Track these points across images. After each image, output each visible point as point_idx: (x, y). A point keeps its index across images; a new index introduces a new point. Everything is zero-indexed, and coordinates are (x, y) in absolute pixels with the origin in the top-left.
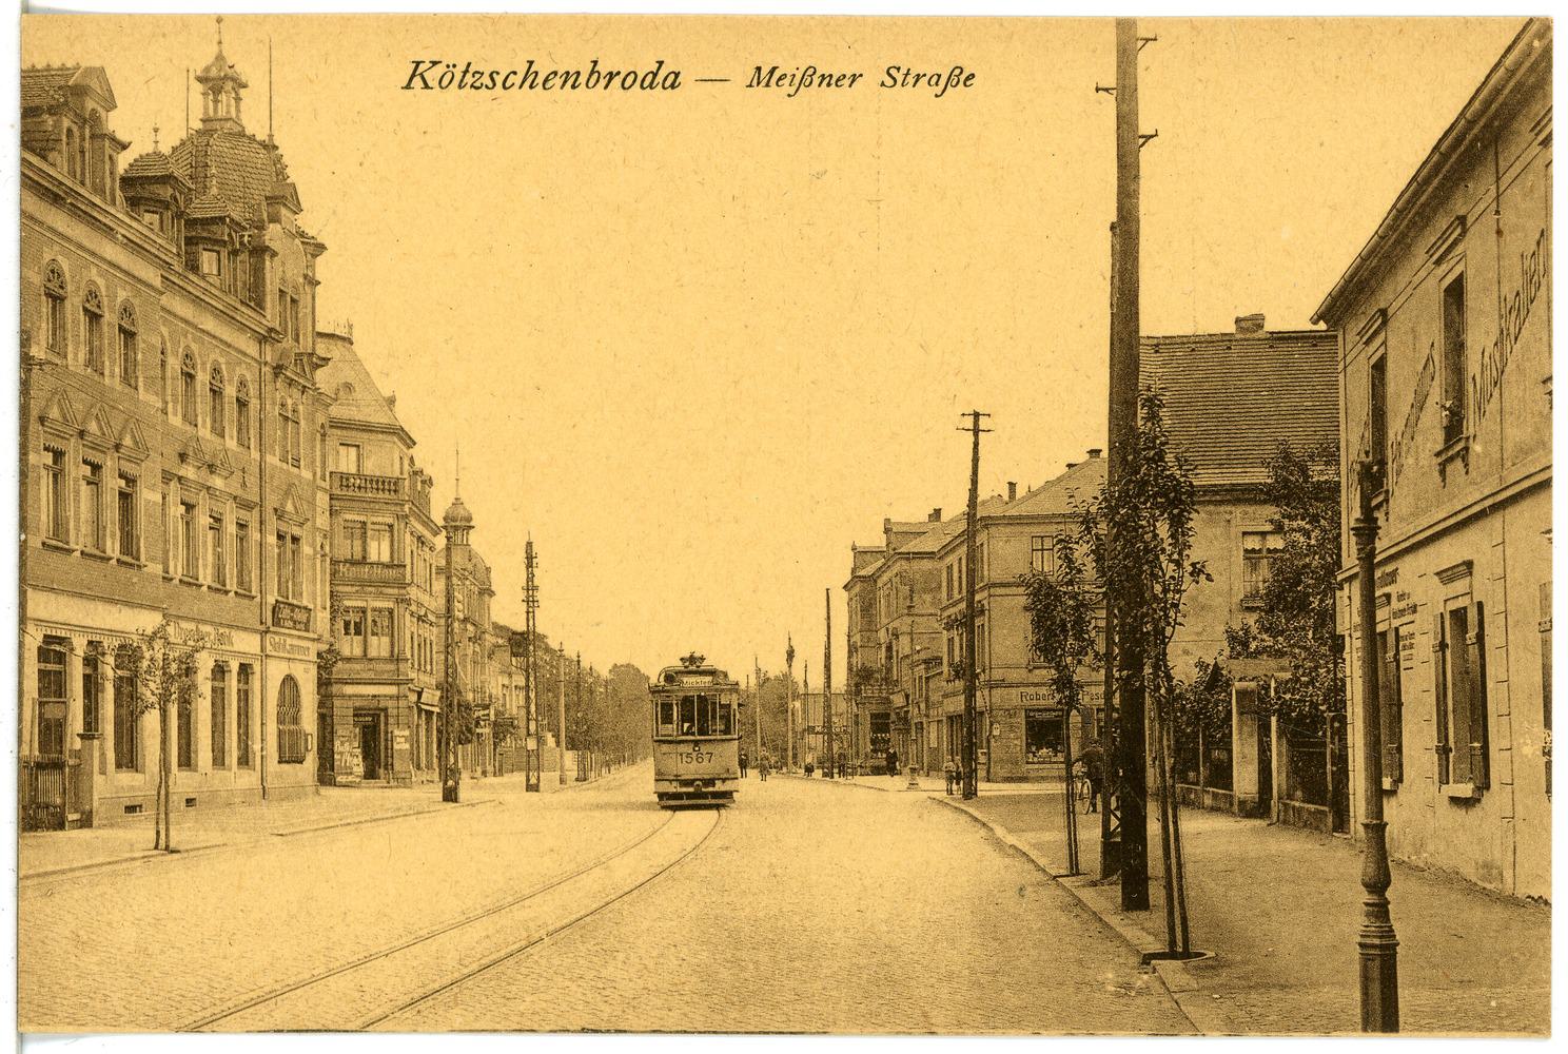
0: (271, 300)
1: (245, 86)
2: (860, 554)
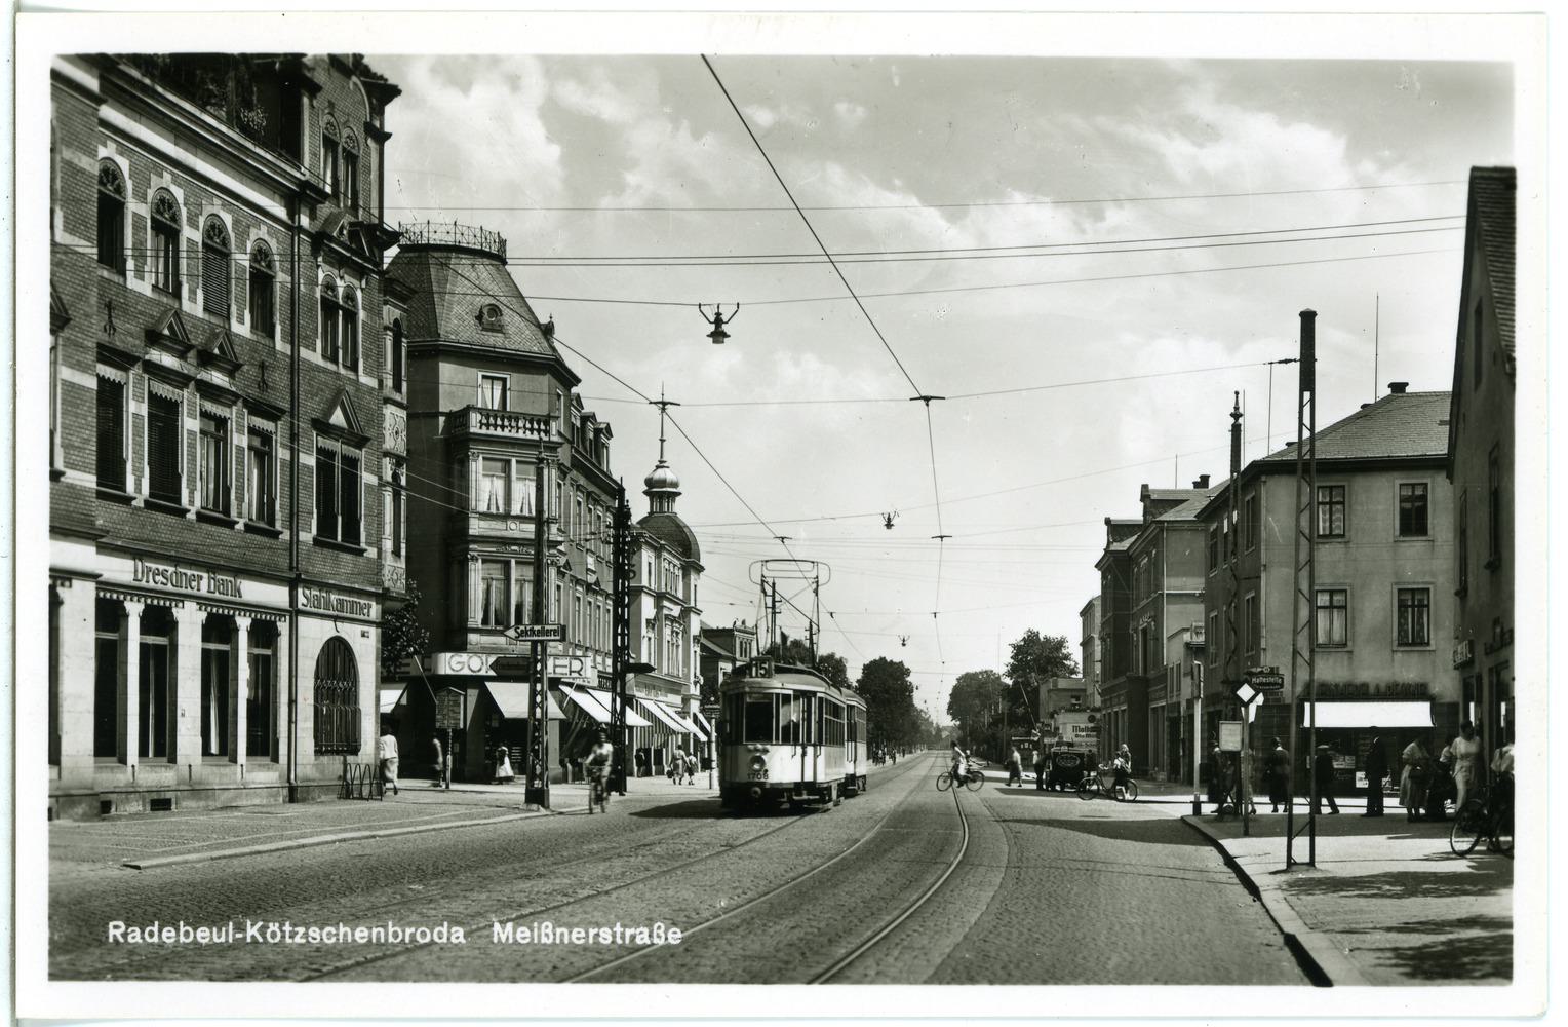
2: (1116, 530)
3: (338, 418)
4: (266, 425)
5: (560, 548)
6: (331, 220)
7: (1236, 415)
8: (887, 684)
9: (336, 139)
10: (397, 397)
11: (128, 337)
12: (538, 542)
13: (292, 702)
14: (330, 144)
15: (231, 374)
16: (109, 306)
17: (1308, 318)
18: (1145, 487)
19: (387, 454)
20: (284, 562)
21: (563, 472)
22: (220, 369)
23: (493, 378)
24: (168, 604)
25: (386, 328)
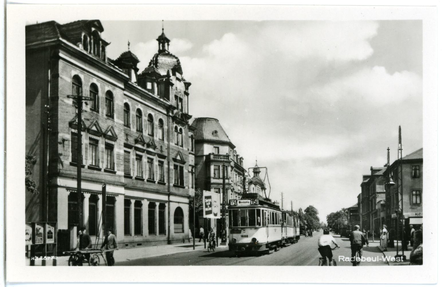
3: (178, 158)
6: (176, 113)
9: (178, 95)
11: (131, 141)
12: (224, 184)
13: (169, 222)
14: (176, 97)
19: (190, 165)
20: (167, 190)
21: (232, 167)
22: (152, 148)
24: (140, 200)
25: (189, 137)
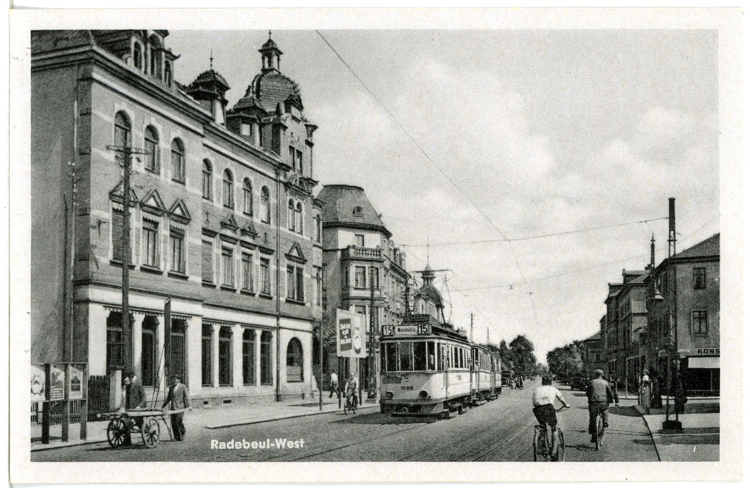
0: (284, 150)
1: (281, 53)
2: (612, 287)
4: (266, 256)
5: (385, 300)
7: (653, 241)
8: (520, 350)
10: (318, 244)
11: (214, 225)
14: (292, 148)
15: (254, 238)
16: (207, 214)
17: (672, 201)
18: (624, 270)
23: (359, 235)
25: (314, 218)
